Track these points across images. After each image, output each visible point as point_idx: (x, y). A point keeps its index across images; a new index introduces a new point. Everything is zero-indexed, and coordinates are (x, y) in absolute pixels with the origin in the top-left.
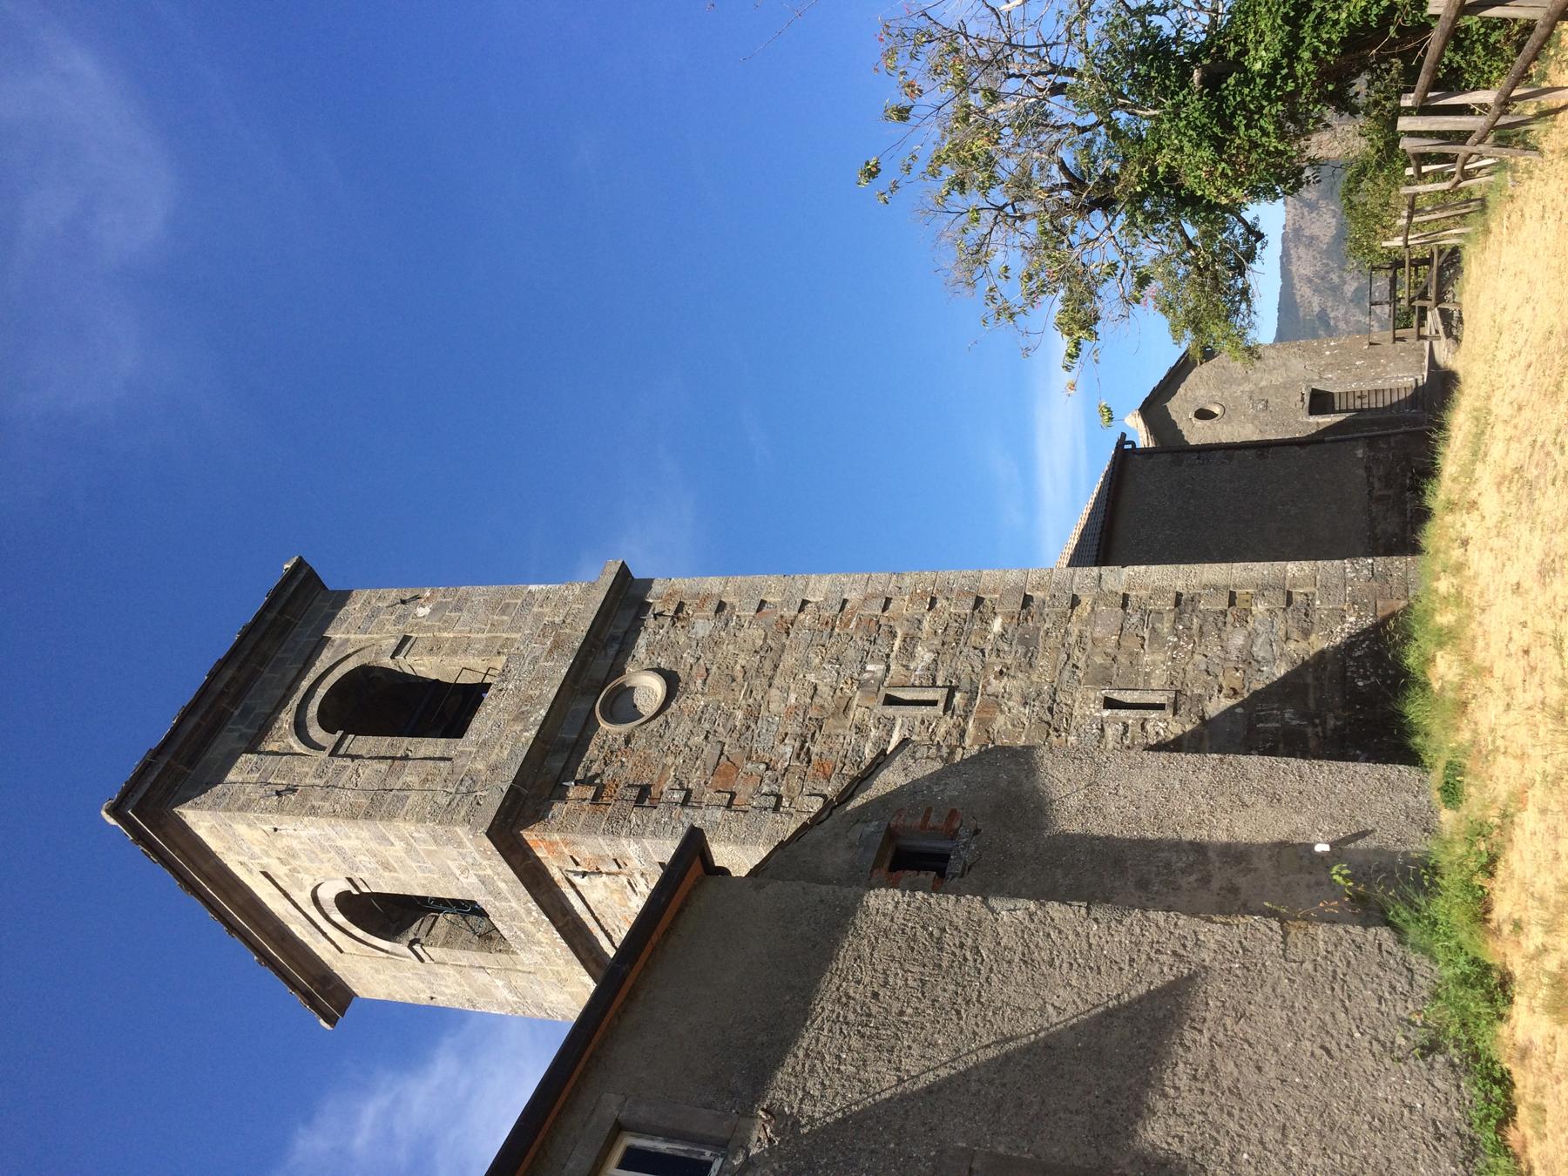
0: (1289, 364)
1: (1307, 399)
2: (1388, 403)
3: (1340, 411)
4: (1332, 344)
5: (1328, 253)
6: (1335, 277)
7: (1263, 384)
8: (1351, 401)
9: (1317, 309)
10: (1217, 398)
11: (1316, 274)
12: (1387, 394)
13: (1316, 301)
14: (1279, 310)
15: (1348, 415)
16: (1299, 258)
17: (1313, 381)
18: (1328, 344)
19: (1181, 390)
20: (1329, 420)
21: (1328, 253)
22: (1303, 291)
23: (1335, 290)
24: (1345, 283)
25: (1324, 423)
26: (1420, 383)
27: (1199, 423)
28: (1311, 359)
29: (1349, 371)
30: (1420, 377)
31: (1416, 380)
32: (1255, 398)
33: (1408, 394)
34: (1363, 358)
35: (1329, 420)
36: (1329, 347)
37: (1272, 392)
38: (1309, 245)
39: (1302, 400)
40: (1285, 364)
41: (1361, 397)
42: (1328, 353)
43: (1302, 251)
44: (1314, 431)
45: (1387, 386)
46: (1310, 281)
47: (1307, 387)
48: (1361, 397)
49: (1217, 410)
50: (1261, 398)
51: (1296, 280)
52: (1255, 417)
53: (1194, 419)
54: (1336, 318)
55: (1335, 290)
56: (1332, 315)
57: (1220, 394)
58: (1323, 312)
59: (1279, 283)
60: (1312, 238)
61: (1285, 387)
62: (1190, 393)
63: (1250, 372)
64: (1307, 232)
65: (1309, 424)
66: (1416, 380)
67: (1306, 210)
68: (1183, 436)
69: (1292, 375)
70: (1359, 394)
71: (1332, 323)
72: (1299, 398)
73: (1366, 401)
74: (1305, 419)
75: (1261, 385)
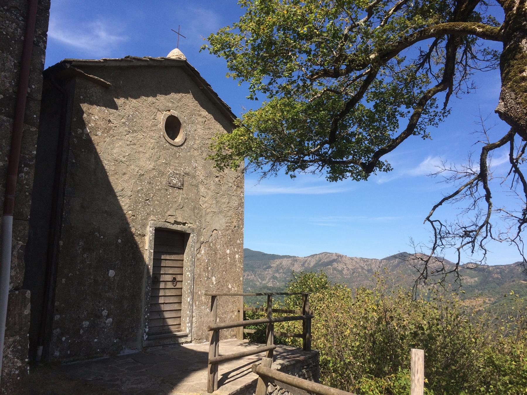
0: (221, 216)
1: (179, 228)
2: (164, 307)
3: (157, 260)
4: (237, 256)
5: (289, 269)
6: (281, 271)
7: (202, 189)
8: (171, 271)
9: (272, 265)
10: (190, 143)
11: (283, 266)
12: (176, 307)
13: (275, 265)
14: (273, 255)
15: (151, 267)
16: (288, 261)
17: (199, 234)
18: (237, 252)
19: (205, 113)
20: (147, 247)
21: (289, 269)
22: (278, 262)
23: (277, 271)
24: (279, 274)
25: (144, 243)
26: (183, 340)
27: (162, 118)
28: (224, 236)
29: (206, 270)
30: (189, 339)
31: (186, 336)
32: (186, 178)
33: (173, 328)
34: (218, 282)
35: (147, 247)
36: (233, 254)
37: (192, 195)
38: (291, 264)
39: (176, 223)
40: (220, 212)
41: (174, 280)
42: (228, 252)
43: (290, 262)
44: (133, 230)
45: (184, 306)
46: (281, 264)
47: (193, 230)
48: (174, 280)
49: (179, 140)
50: (186, 184)
51: (282, 260)
52: (162, 174)
53: (169, 114)
54: (269, 271)
55: (277, 271)
56: (270, 270)
57: (195, 146)
58: (270, 267)
59: (281, 254)
60: (294, 265)
61: (195, 208)
62: (201, 119)
63: (217, 179)
64: (295, 263)
65: (144, 226)
66: (186, 336)
67: (302, 263)
68: (148, 96)
69: (208, 218)
70: (179, 278)
71: (267, 270)
72: (179, 220)
73: (170, 285)
74: (150, 223)
75: (200, 186)
